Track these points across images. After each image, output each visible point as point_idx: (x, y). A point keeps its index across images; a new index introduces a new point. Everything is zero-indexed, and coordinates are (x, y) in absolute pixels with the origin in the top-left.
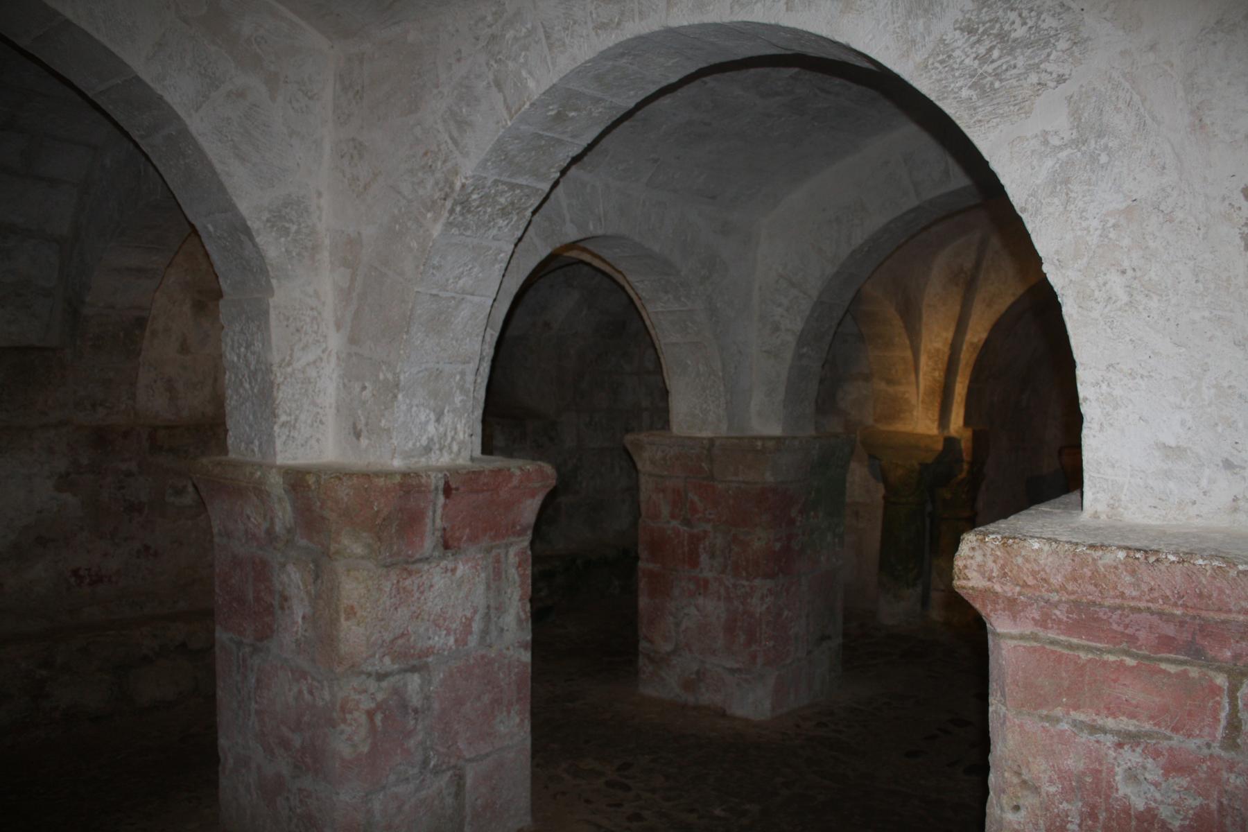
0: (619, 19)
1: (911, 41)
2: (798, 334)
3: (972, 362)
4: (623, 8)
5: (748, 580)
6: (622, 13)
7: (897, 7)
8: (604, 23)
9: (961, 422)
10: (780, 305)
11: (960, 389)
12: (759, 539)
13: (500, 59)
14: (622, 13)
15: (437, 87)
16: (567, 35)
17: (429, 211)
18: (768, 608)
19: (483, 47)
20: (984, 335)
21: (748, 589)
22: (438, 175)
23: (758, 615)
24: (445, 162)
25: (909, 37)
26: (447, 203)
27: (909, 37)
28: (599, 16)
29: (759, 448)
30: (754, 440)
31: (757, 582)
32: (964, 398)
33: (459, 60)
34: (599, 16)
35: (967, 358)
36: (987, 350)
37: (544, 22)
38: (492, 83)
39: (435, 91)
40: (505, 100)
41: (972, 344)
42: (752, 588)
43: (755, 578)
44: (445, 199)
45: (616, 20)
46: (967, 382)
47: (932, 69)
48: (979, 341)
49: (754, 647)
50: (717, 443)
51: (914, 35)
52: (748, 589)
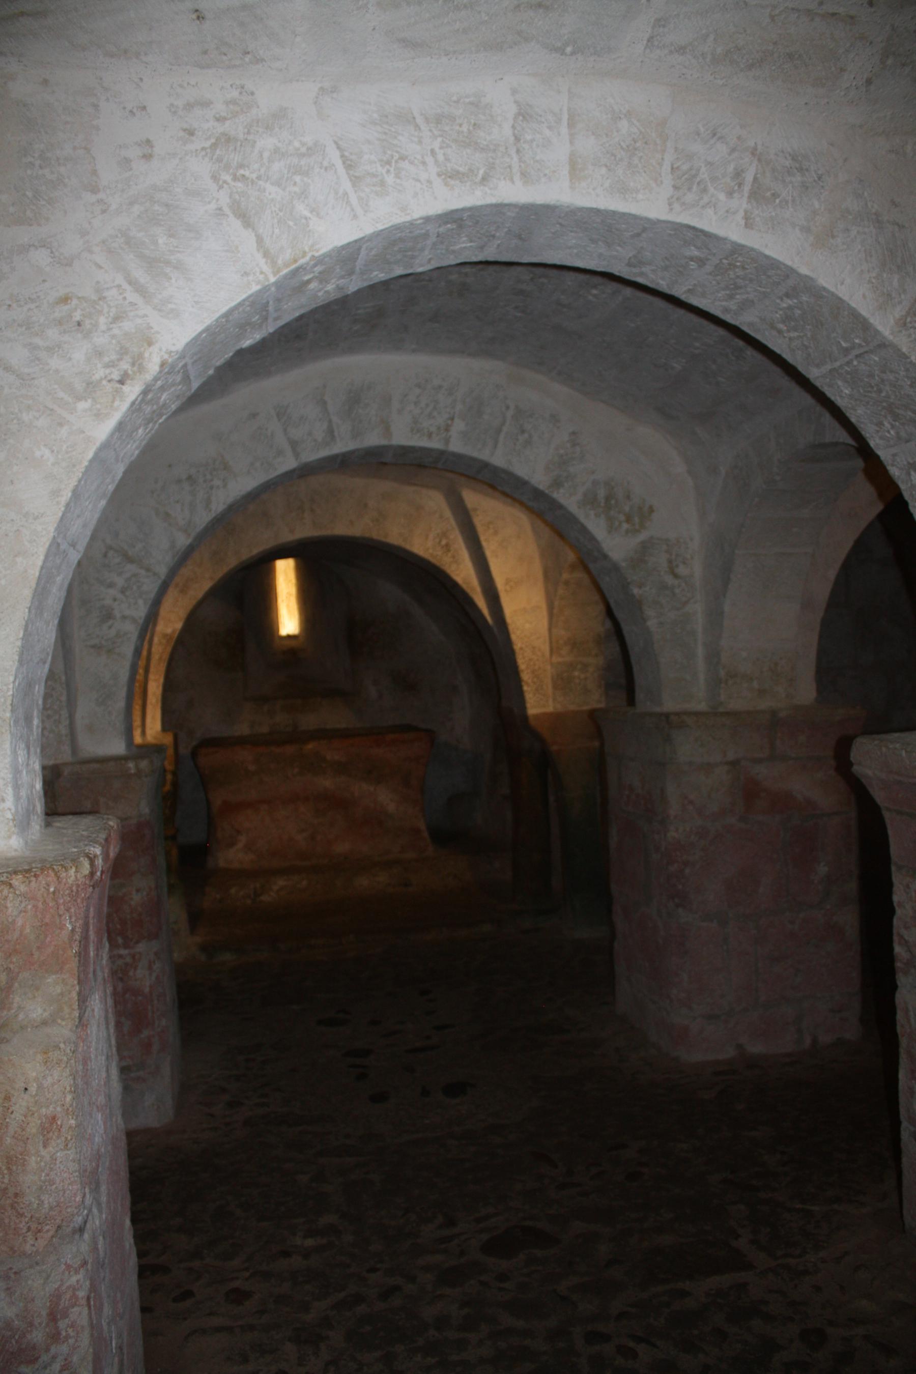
0: (485, 172)
1: (888, 295)
2: (141, 621)
3: (166, 656)
4: (491, 160)
5: (126, 946)
6: (492, 167)
7: (871, 256)
8: (458, 172)
9: (158, 726)
10: (111, 585)
11: (155, 688)
12: (138, 891)
13: (243, 176)
14: (492, 167)
15: (95, 190)
16: (388, 171)
17: (79, 398)
18: (157, 977)
19: (203, 149)
20: (179, 625)
21: (129, 960)
22: (100, 340)
23: (147, 990)
24: (117, 319)
25: (885, 291)
26: (126, 388)
27: (885, 291)
28: (447, 159)
29: (133, 771)
30: (123, 762)
31: (141, 947)
32: (160, 698)
33: (147, 157)
34: (447, 159)
35: (160, 651)
36: (181, 642)
37: (340, 143)
38: (227, 210)
39: (91, 198)
40: (260, 240)
41: (165, 636)
42: (133, 956)
43: (137, 942)
44: (122, 382)
45: (481, 172)
46: (162, 680)
47: (911, 328)
48: (174, 631)
49: (145, 1033)
50: (66, 771)
51: (889, 289)
52: (129, 960)
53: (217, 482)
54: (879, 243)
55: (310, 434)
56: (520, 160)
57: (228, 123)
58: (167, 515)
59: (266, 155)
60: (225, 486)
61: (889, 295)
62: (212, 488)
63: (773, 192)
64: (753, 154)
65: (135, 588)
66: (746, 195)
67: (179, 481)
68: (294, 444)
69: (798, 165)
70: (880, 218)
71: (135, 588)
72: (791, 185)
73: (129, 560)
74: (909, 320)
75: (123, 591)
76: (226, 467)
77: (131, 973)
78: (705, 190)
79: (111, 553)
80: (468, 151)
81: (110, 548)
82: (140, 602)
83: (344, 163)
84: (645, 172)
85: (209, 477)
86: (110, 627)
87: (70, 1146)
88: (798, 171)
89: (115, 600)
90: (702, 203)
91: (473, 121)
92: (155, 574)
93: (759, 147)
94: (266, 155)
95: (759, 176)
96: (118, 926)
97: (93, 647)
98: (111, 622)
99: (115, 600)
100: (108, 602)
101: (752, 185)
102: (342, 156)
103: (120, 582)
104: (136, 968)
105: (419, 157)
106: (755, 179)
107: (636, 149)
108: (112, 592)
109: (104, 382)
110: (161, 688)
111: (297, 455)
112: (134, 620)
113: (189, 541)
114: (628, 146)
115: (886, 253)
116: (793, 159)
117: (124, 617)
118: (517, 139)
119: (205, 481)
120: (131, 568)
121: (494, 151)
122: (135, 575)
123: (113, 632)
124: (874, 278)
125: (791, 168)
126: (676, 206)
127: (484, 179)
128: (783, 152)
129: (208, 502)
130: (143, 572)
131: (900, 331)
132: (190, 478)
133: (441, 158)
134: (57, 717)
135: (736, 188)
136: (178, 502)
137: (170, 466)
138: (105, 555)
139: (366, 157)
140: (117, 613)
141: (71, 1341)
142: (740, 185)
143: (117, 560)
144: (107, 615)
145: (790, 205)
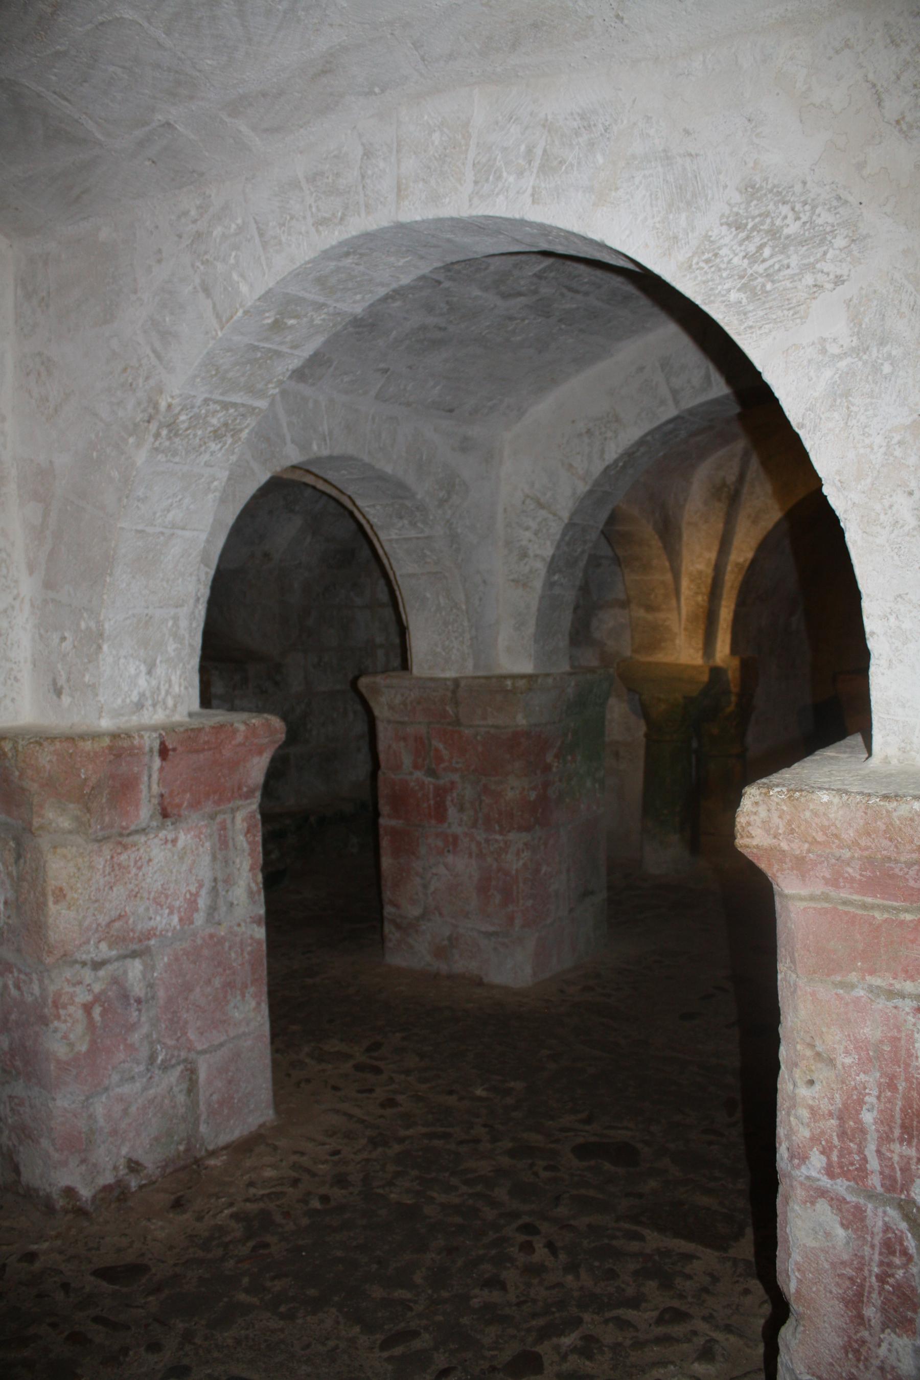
1: (674, 238)
2: (548, 559)
3: (737, 584)
5: (501, 833)
6: (346, 207)
7: (657, 199)
10: (527, 529)
11: (726, 614)
14: (346, 207)
15: (135, 292)
16: (284, 232)
17: (131, 435)
20: (750, 555)
21: (502, 845)
23: (514, 872)
24: (147, 378)
25: (671, 233)
28: (319, 210)
29: (509, 688)
31: (512, 836)
33: (159, 261)
34: (319, 210)
35: (732, 581)
41: (737, 564)
42: (506, 843)
43: (509, 831)
44: (149, 422)
48: (745, 561)
51: (675, 231)
52: (502, 845)
53: (609, 434)
54: (667, 182)
55: (689, 381)
56: (365, 195)
57: (199, 222)
58: (571, 466)
59: (218, 240)
60: (616, 437)
61: (675, 238)
62: (606, 439)
63: (560, 159)
64: (544, 126)
65: (544, 530)
66: (535, 171)
67: (580, 435)
68: (675, 393)
69: (586, 124)
70: (669, 154)
71: (544, 530)
72: (577, 147)
73: (541, 506)
74: (694, 261)
75: (536, 534)
76: (617, 419)
77: (503, 856)
78: (499, 178)
79: (528, 501)
80: (332, 198)
81: (527, 496)
82: (548, 543)
83: (259, 233)
84: (452, 176)
85: (603, 429)
86: (526, 564)
87: (72, 908)
88: (586, 129)
89: (530, 541)
90: (497, 190)
91: (335, 172)
92: (560, 518)
93: (549, 117)
94: (218, 240)
95: (548, 147)
96: (497, 816)
97: (513, 581)
98: (526, 559)
99: (530, 541)
100: (524, 543)
101: (541, 160)
102: (258, 228)
103: (534, 525)
104: (507, 853)
105: (301, 214)
106: (545, 151)
107: (446, 156)
108: (528, 534)
109: (141, 423)
110: (731, 614)
111: (677, 402)
112: (544, 559)
113: (587, 488)
114: (440, 156)
115: (674, 190)
116: (582, 118)
117: (536, 556)
118: (363, 177)
119: (601, 434)
120: (543, 513)
121: (349, 192)
122: (545, 520)
123: (527, 568)
124: (659, 222)
125: (579, 128)
126: (476, 201)
127: (342, 219)
128: (572, 114)
129: (602, 452)
130: (551, 516)
131: (684, 276)
132: (588, 431)
133: (314, 209)
134: (461, 639)
135: (527, 166)
136: (578, 453)
137: (573, 422)
138: (523, 503)
139: (271, 224)
140: (531, 553)
141: (69, 1025)
142: (530, 162)
143: (532, 507)
144: (524, 555)
145: (575, 168)
